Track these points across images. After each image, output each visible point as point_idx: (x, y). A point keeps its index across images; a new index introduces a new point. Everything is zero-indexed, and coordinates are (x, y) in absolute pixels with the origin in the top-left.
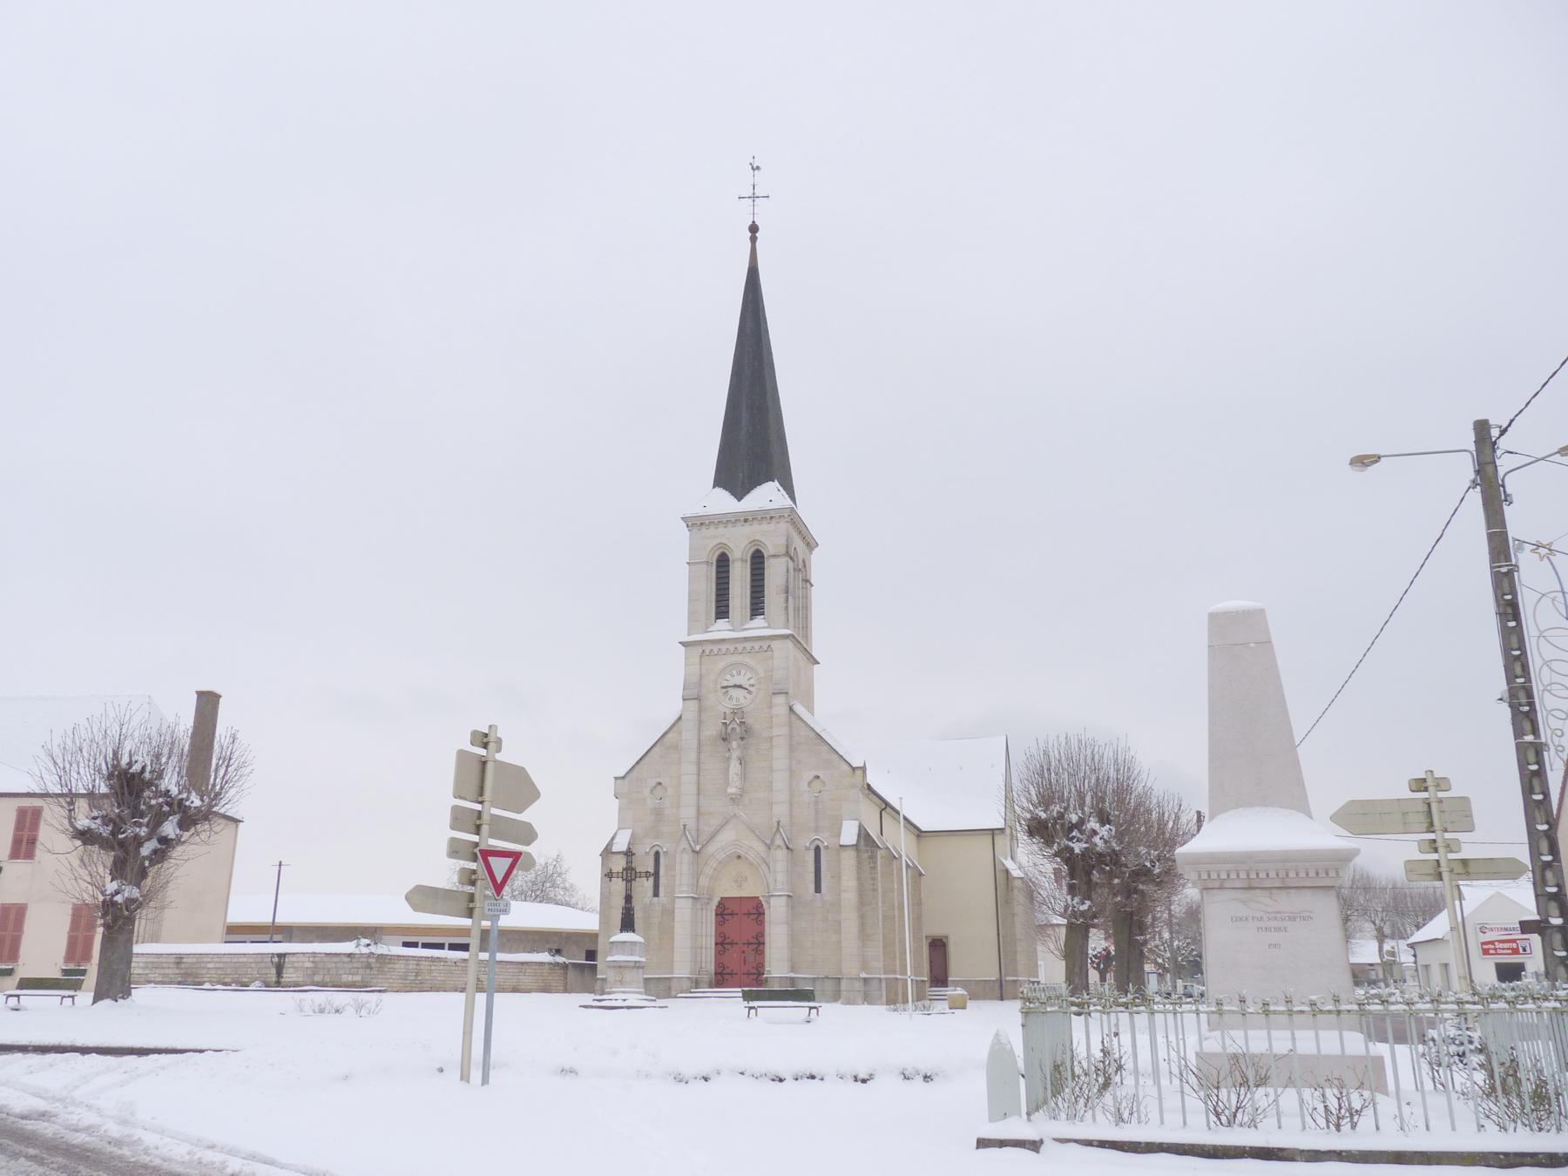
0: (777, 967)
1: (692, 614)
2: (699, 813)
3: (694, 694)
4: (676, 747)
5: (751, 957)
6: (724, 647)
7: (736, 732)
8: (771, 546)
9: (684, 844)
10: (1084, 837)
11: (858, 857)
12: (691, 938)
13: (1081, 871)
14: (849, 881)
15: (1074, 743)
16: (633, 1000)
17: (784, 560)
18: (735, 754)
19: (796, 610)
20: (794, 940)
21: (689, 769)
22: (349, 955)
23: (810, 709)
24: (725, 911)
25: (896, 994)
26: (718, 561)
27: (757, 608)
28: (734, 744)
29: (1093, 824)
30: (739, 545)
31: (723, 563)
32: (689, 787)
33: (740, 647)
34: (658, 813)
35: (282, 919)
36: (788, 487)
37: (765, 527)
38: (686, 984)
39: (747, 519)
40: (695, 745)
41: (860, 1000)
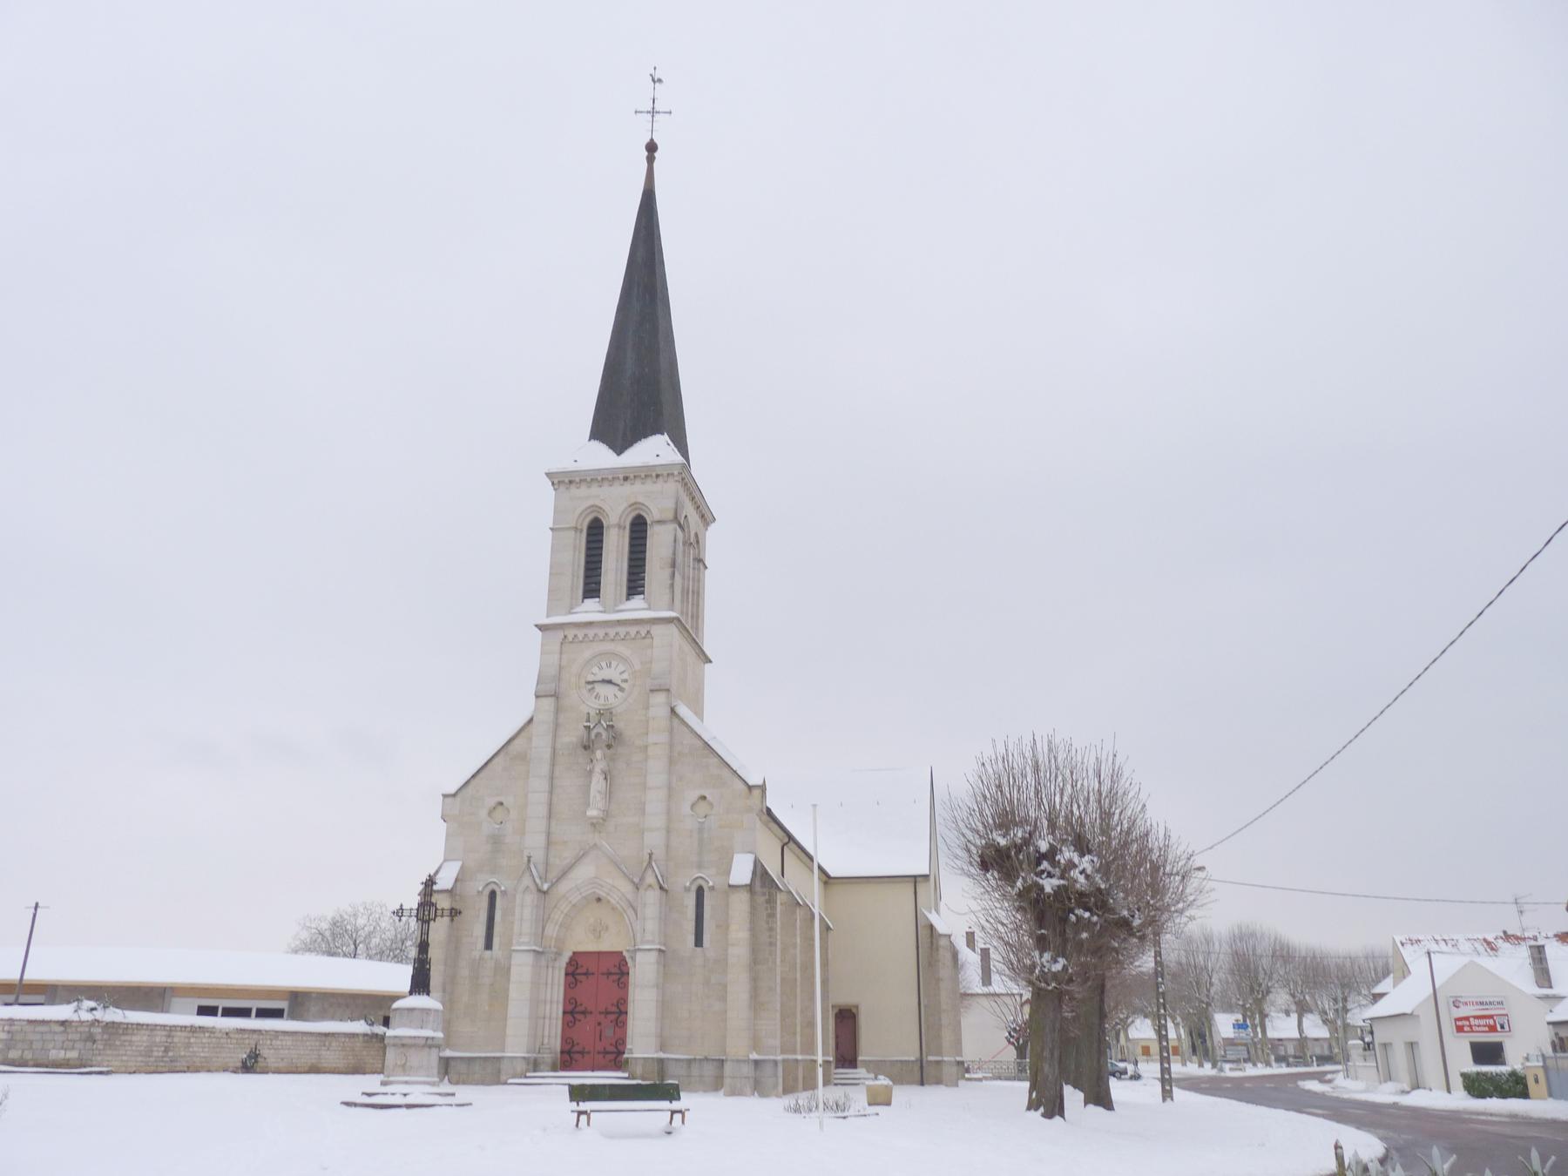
0: (641, 1043)
1: (553, 591)
2: (549, 843)
3: (550, 691)
4: (523, 758)
5: (609, 1032)
6: (591, 632)
7: (602, 739)
8: (653, 512)
9: (527, 881)
10: (1057, 872)
11: (752, 900)
12: (530, 1005)
13: (1048, 916)
14: (739, 932)
15: (1042, 748)
16: (418, 1094)
17: (672, 527)
18: (599, 766)
19: (685, 592)
20: (665, 1008)
21: (539, 785)
22: (63, 1023)
23: (699, 713)
24: (579, 969)
25: (796, 1080)
26: (590, 528)
27: (635, 585)
28: (599, 754)
29: (1067, 854)
30: (615, 507)
31: (595, 531)
32: (538, 808)
33: (612, 632)
34: (496, 841)
35: (32, 975)
36: (680, 443)
37: (650, 486)
38: (520, 1066)
39: (628, 476)
40: (547, 755)
41: (748, 1090)
